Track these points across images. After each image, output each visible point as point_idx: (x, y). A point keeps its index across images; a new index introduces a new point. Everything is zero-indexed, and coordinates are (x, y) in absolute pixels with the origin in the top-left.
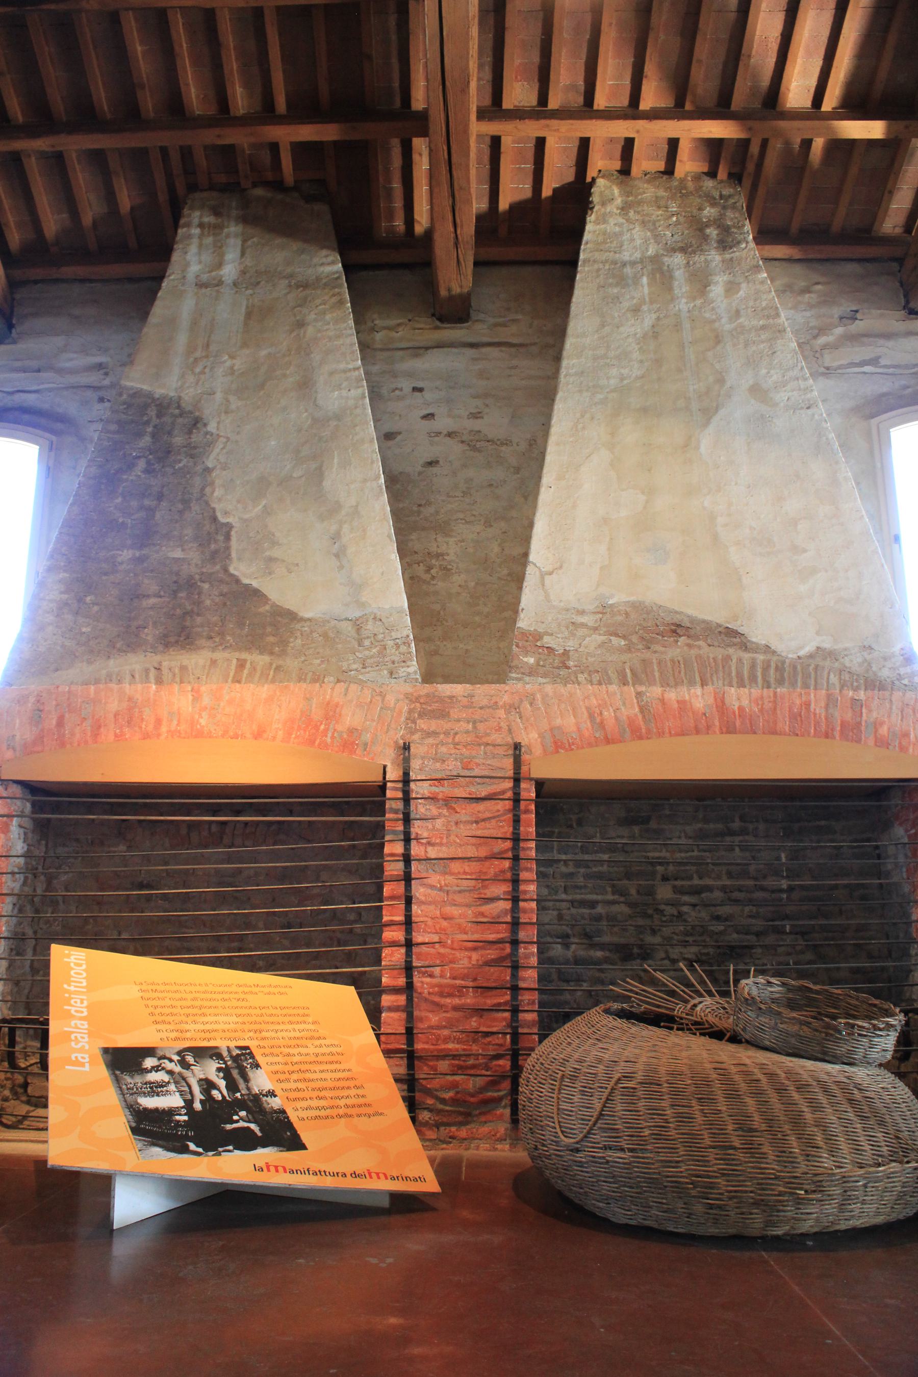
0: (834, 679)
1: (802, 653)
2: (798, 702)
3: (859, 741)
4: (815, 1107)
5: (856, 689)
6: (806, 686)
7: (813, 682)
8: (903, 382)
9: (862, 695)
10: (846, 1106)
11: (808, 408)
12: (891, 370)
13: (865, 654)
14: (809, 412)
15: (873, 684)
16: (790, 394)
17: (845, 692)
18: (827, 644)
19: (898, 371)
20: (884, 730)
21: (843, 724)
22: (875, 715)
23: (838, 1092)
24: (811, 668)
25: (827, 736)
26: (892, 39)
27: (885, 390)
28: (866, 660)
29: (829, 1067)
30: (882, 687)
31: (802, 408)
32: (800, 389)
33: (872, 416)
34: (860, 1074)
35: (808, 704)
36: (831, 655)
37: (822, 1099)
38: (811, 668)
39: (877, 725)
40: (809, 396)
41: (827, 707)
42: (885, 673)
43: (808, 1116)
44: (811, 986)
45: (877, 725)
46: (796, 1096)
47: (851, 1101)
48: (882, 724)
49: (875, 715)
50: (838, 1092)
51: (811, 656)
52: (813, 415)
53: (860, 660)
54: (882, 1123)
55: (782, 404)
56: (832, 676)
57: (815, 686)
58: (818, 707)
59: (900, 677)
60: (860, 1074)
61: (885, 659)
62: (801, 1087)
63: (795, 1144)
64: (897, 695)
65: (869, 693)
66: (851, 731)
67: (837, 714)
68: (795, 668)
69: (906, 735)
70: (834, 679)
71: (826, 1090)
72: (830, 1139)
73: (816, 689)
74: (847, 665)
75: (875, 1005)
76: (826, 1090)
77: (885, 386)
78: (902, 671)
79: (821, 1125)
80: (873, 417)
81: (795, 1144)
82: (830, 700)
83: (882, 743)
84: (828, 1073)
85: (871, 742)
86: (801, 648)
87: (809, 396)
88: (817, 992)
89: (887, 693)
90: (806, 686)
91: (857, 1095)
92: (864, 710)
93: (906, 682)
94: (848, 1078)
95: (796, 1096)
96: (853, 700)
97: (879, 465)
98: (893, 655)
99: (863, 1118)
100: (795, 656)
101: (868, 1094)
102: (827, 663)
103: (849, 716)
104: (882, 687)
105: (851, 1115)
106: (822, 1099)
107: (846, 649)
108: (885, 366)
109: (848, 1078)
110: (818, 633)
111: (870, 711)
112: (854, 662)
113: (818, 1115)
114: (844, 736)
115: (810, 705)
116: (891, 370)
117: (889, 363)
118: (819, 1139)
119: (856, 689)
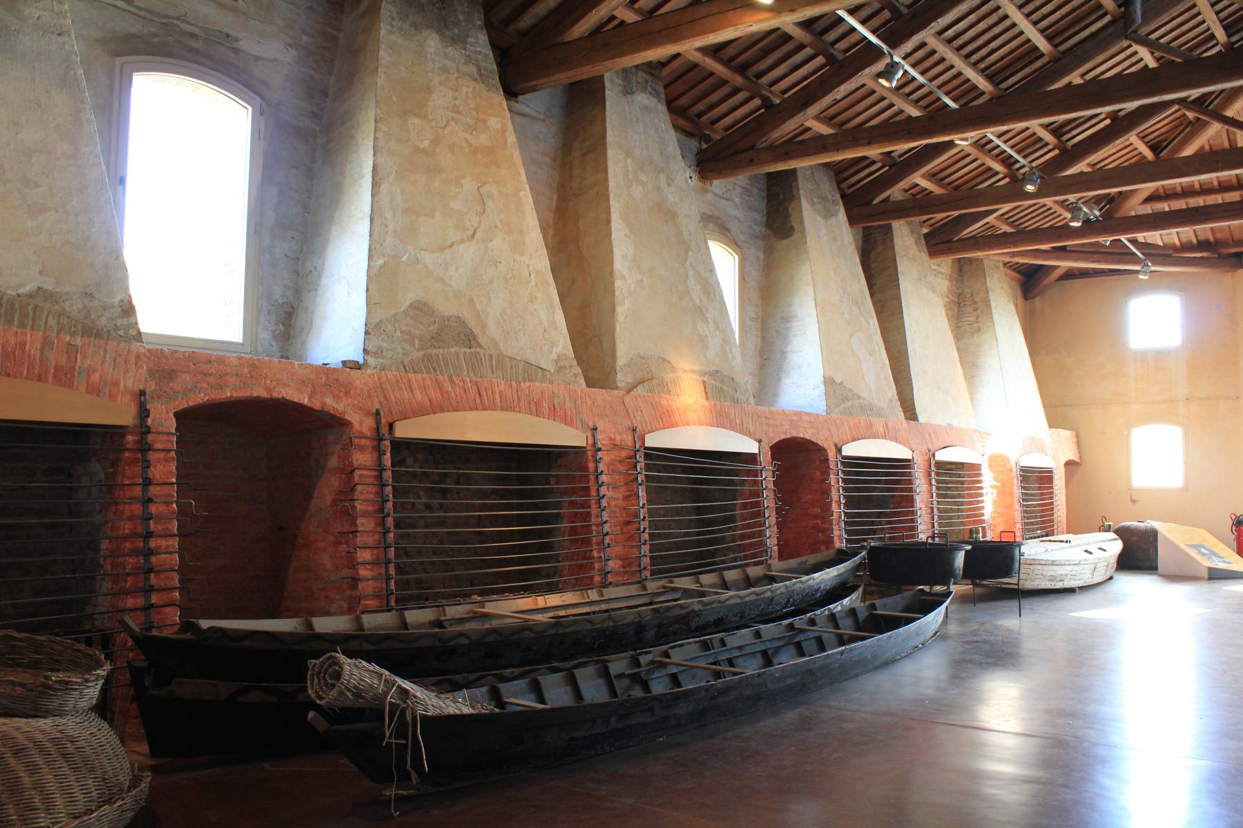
0: (52, 321)
1: (22, 291)
2: (13, 341)
3: (70, 386)
4: (33, 769)
5: (74, 334)
6: (23, 325)
7: (30, 323)
8: (153, 30)
9: (78, 341)
10: (61, 762)
11: (59, 35)
12: (143, 13)
13: (86, 301)
14: (59, 39)
15: (90, 331)
16: (42, 13)
17: (62, 335)
18: (49, 285)
19: (149, 16)
20: (96, 378)
21: (57, 369)
22: (88, 362)
23: (52, 750)
24: (30, 308)
25: (40, 379)
26: (534, 83)
27: (134, 31)
28: (85, 307)
29: (41, 723)
30: (98, 335)
31: (52, 33)
32: (53, 11)
33: (118, 54)
34: (70, 724)
35: (23, 345)
36: (51, 296)
37: (39, 760)
38: (30, 308)
39: (90, 371)
40: (62, 21)
41: (42, 349)
42: (103, 322)
43: (26, 780)
44: (15, 634)
45: (90, 371)
46: (13, 762)
47: (65, 756)
48: (95, 371)
49: (88, 362)
50: (52, 750)
51: (31, 295)
52: (64, 44)
53: (80, 306)
54: (92, 770)
55: (31, 21)
56: (51, 318)
57: (33, 325)
58: (33, 348)
59: (116, 328)
60: (70, 724)
61: (105, 308)
62: (19, 752)
63: (12, 811)
64: (112, 345)
65: (86, 339)
66: (65, 376)
67: (52, 358)
68: (12, 305)
69: (116, 383)
70: (52, 321)
71: (42, 750)
72: (47, 800)
73: (32, 330)
74: (67, 309)
75: (79, 651)
76: (42, 750)
77: (136, 28)
78: (119, 322)
79: (39, 787)
80: (118, 56)
81: (12, 811)
82: (46, 342)
83: (93, 390)
84: (43, 732)
85: (83, 388)
86: (22, 286)
87: (62, 21)
88: (21, 640)
89: (102, 342)
90: (23, 325)
91: (70, 748)
92: (79, 356)
93: (121, 333)
94: (61, 732)
95: (13, 762)
96: (69, 344)
97: (116, 105)
98: (113, 306)
99: (76, 769)
100: (14, 293)
101: (79, 744)
102: (47, 305)
103: (63, 360)
104: (98, 335)
105: (66, 770)
106: (39, 760)
107: (67, 294)
108: (138, 7)
109: (61, 732)
110: (40, 273)
111: (85, 357)
112: (74, 307)
113: (35, 777)
114: (57, 380)
115: (25, 344)
116: (143, 13)
117: (142, 5)
118: (37, 801)
119: (74, 334)
